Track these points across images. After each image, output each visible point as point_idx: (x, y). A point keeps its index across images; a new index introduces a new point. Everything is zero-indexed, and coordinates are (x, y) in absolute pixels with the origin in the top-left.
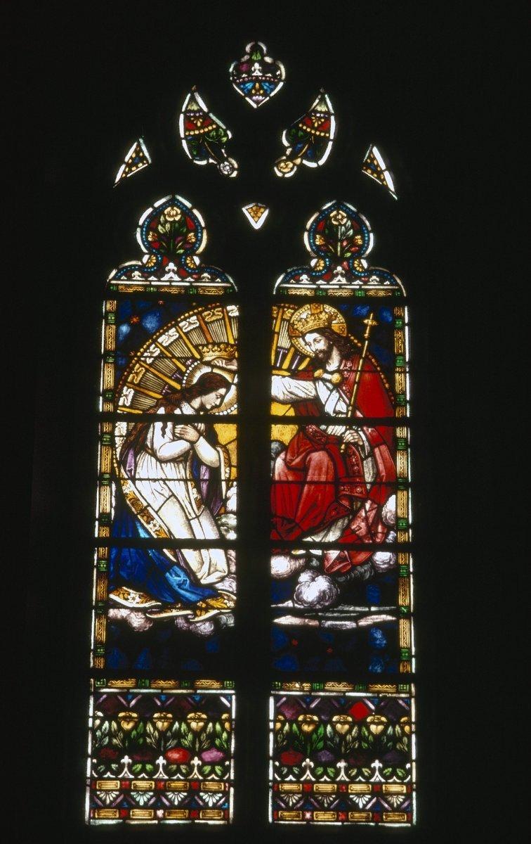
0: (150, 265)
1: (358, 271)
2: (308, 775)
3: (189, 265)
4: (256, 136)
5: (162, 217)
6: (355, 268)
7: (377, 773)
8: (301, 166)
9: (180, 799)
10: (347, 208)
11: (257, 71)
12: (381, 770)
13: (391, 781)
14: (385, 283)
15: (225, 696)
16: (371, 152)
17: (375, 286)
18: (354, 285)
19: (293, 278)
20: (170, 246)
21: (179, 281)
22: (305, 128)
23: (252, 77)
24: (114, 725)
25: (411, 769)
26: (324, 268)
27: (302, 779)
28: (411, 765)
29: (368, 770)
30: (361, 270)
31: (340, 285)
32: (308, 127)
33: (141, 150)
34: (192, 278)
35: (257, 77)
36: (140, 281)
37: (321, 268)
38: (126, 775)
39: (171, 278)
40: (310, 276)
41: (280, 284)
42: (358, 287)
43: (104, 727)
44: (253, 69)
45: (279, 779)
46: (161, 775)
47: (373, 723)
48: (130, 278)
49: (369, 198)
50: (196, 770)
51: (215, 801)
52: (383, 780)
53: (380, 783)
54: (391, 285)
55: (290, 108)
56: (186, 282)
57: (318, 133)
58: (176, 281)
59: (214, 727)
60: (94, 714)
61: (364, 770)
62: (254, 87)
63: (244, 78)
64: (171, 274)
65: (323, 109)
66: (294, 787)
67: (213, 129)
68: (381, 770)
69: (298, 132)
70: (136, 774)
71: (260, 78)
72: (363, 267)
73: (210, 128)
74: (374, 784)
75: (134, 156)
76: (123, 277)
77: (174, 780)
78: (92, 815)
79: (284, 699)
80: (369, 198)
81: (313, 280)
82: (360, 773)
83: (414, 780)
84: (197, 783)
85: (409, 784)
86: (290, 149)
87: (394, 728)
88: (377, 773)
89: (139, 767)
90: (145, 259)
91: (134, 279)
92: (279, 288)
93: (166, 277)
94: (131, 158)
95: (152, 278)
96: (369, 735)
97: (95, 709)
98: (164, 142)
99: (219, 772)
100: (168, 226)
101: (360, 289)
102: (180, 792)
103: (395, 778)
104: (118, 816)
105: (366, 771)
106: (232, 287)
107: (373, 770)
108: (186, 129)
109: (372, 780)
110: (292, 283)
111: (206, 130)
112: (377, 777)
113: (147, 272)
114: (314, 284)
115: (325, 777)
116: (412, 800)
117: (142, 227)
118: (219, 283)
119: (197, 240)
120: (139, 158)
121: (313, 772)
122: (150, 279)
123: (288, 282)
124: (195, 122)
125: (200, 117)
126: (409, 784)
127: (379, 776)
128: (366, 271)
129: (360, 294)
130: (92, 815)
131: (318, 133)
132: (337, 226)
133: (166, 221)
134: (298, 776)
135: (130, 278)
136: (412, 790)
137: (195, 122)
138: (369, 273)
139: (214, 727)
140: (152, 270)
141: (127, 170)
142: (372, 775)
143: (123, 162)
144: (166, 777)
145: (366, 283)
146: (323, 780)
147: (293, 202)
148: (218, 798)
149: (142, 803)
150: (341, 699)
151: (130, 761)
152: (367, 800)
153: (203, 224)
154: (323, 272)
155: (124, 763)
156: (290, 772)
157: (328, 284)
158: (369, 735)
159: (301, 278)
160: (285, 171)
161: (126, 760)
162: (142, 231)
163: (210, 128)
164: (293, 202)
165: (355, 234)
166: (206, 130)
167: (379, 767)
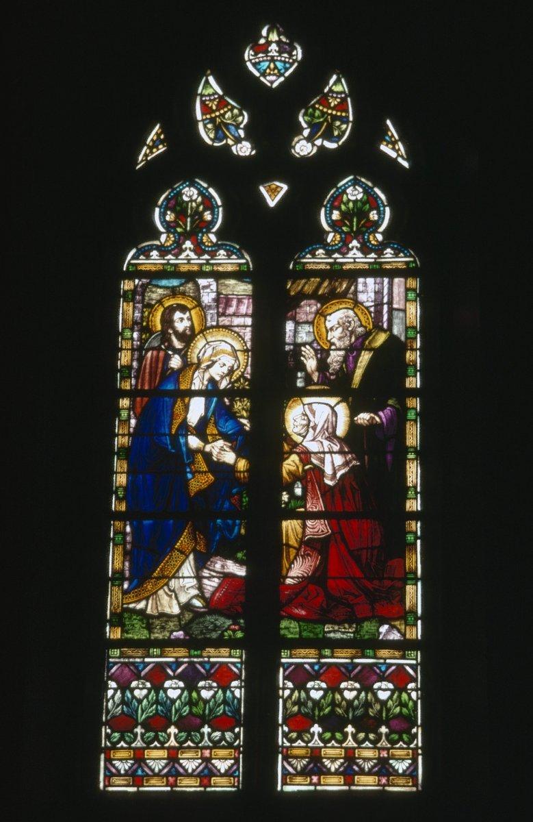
0: (169, 244)
4: (273, 114)
5: (345, 196)
6: (204, 244)
8: (322, 148)
9: (370, 766)
13: (329, 745)
14: (232, 257)
15: (234, 664)
20: (191, 226)
21: (362, 258)
22: (321, 108)
24: (303, 694)
25: (416, 734)
28: (417, 730)
30: (210, 244)
32: (324, 107)
35: (272, 57)
37: (337, 242)
38: (384, 744)
39: (188, 255)
41: (131, 260)
43: (360, 697)
44: (270, 49)
46: (139, 744)
47: (313, 688)
48: (148, 257)
49: (382, 171)
50: (350, 738)
54: (406, 256)
55: (304, 87)
56: (202, 259)
57: (334, 113)
58: (194, 259)
59: (366, 696)
60: (284, 684)
62: (269, 67)
64: (188, 252)
66: (338, 751)
68: (387, 736)
69: (315, 112)
70: (325, 742)
71: (272, 60)
72: (211, 242)
74: (312, 748)
75: (155, 138)
76: (142, 257)
77: (396, 748)
79: (393, 668)
80: (382, 171)
81: (329, 254)
82: (156, 738)
83: (420, 745)
84: (142, 751)
86: (308, 130)
90: (163, 238)
91: (219, 257)
94: (152, 140)
95: (336, 255)
96: (342, 701)
97: (285, 678)
99: (161, 739)
100: (351, 205)
101: (208, 263)
102: (403, 760)
103: (333, 742)
104: (342, 783)
105: (228, 735)
107: (313, 735)
108: (203, 114)
109: (133, 745)
110: (309, 258)
112: (350, 742)
113: (164, 251)
114: (331, 258)
115: (156, 743)
116: (239, 764)
117: (218, 207)
118: (235, 260)
119: (379, 217)
120: (155, 145)
125: (215, 99)
128: (215, 245)
130: (107, 783)
131: (334, 113)
132: (187, 203)
133: (349, 200)
134: (375, 742)
135: (148, 257)
138: (218, 247)
139: (366, 696)
140: (207, 249)
141: (148, 151)
142: (135, 740)
143: (145, 144)
144: (389, 746)
147: (314, 179)
148: (197, 765)
150: (349, 666)
151: (387, 730)
153: (219, 203)
156: (300, 737)
158: (342, 701)
159: (151, 254)
160: (303, 148)
162: (326, 211)
164: (314, 179)
165: (205, 210)
167: (175, 733)
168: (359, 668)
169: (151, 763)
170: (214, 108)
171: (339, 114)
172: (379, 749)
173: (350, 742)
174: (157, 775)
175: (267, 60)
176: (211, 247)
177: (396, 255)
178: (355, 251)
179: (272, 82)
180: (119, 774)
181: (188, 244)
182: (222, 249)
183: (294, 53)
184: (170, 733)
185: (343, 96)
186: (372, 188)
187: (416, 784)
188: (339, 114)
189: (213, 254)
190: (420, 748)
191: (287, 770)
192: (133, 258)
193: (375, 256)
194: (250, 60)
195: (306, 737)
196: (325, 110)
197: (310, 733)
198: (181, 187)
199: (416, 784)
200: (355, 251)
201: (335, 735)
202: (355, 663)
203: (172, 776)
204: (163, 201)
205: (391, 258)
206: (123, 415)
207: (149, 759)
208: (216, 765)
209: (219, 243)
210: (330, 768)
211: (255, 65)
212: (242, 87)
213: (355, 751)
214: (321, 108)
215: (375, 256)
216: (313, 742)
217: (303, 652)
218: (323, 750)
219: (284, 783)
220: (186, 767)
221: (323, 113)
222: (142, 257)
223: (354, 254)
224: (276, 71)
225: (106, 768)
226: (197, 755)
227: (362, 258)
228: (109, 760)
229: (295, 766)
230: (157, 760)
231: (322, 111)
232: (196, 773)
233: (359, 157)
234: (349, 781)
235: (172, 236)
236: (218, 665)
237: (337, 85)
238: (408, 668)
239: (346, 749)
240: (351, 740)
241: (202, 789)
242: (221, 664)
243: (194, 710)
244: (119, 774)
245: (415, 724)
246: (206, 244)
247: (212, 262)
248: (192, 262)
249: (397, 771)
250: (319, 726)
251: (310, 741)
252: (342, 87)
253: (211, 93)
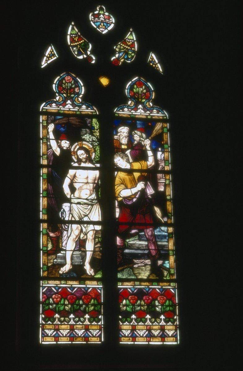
1: (148, 107)
2: (72, 322)
3: (148, 106)
4: (104, 45)
7: (72, 320)
10: (72, 75)
11: (102, 18)
12: (74, 319)
16: (151, 56)
17: (155, 114)
18: (75, 109)
19: (49, 104)
21: (72, 109)
23: (100, 20)
26: (62, 101)
27: (54, 323)
29: (83, 319)
31: (70, 109)
32: (125, 45)
33: (53, 51)
34: (149, 112)
35: (102, 20)
36: (56, 108)
39: (69, 107)
40: (128, 109)
42: (77, 110)
45: (44, 323)
46: (72, 323)
51: (157, 334)
52: (74, 323)
53: (74, 325)
54: (162, 114)
55: (117, 35)
56: (147, 113)
61: (81, 318)
63: (97, 20)
65: (131, 38)
67: (83, 42)
70: (76, 322)
71: (103, 21)
73: (82, 42)
74: (161, 326)
76: (121, 110)
77: (78, 325)
78: (42, 340)
83: (103, 323)
85: (176, 326)
87: (141, 302)
88: (72, 320)
89: (77, 319)
92: (43, 109)
93: (67, 107)
94: (49, 54)
95: (61, 107)
98: (63, 48)
101: (78, 111)
102: (157, 330)
103: (126, 322)
105: (82, 319)
106: (166, 116)
107: (161, 320)
110: (121, 112)
111: (80, 42)
117: (55, 84)
118: (160, 115)
120: (52, 55)
121: (59, 320)
122: (60, 107)
123: (119, 111)
124: (75, 39)
126: (176, 326)
127: (73, 321)
129: (149, 117)
130: (42, 340)
136: (177, 328)
137: (75, 39)
144: (60, 323)
145: (151, 112)
146: (48, 323)
148: (144, 332)
149: (170, 335)
152: (52, 332)
153: (82, 84)
154: (62, 102)
155: (133, 318)
157: (136, 112)
161: (72, 316)
163: (82, 42)
166: (80, 42)
168: (76, 289)
169: (62, 331)
170: (76, 40)
171: (74, 44)
172: (55, 325)
173: (72, 322)
174: (80, 337)
175: (100, 22)
176: (79, 104)
177: (87, 109)
178: (69, 105)
179: (102, 31)
180: (47, 336)
181: (69, 102)
182: (155, 109)
183: (111, 19)
184: (86, 318)
185: (133, 41)
186: (76, 78)
187: (176, 341)
188: (74, 44)
189: (80, 107)
190: (103, 325)
191: (59, 335)
192: (44, 106)
193: (149, 113)
194: (92, 21)
195: (158, 320)
196: (125, 46)
197: (160, 319)
198: (64, 76)
199: (100, 341)
200: (69, 105)
201: (127, 319)
202: (73, 287)
203: (149, 337)
204: (57, 82)
205: (155, 114)
206: (45, 176)
207: (61, 329)
208: (46, 332)
209: (154, 106)
210: (48, 334)
211: (94, 23)
212: (88, 32)
213: (136, 326)
214: (123, 45)
215: (149, 113)
216: (85, 322)
217: (127, 283)
218: (166, 326)
219: (174, 339)
220: (63, 333)
221: (124, 48)
222: (48, 106)
223: (140, 111)
224: (104, 27)
225: (42, 334)
226: (53, 328)
227: (72, 109)
228: (43, 330)
229: (93, 333)
230: (142, 332)
231: (124, 47)
232: (52, 335)
233: (140, 67)
234: (163, 340)
235: (133, 103)
236: (122, 289)
237: (131, 37)
238: (44, 290)
239: (70, 325)
240: (149, 322)
241: (70, 343)
242: (168, 289)
243: (96, 308)
244: (47, 336)
245: (175, 314)
246: (77, 102)
247: (151, 114)
248: (71, 109)
249: (154, 335)
250: (86, 315)
251: (160, 322)
252: (134, 37)
253: (131, 39)
